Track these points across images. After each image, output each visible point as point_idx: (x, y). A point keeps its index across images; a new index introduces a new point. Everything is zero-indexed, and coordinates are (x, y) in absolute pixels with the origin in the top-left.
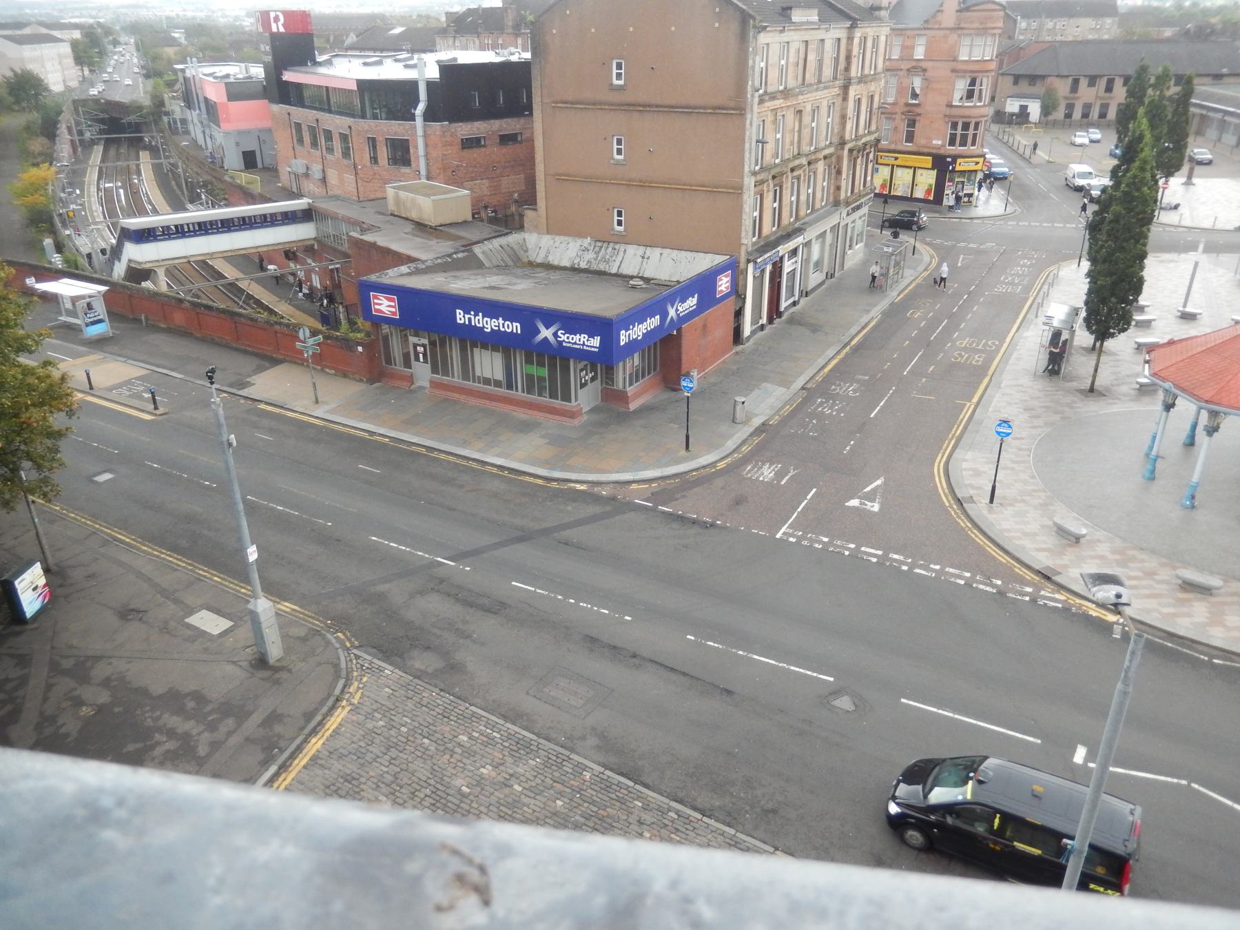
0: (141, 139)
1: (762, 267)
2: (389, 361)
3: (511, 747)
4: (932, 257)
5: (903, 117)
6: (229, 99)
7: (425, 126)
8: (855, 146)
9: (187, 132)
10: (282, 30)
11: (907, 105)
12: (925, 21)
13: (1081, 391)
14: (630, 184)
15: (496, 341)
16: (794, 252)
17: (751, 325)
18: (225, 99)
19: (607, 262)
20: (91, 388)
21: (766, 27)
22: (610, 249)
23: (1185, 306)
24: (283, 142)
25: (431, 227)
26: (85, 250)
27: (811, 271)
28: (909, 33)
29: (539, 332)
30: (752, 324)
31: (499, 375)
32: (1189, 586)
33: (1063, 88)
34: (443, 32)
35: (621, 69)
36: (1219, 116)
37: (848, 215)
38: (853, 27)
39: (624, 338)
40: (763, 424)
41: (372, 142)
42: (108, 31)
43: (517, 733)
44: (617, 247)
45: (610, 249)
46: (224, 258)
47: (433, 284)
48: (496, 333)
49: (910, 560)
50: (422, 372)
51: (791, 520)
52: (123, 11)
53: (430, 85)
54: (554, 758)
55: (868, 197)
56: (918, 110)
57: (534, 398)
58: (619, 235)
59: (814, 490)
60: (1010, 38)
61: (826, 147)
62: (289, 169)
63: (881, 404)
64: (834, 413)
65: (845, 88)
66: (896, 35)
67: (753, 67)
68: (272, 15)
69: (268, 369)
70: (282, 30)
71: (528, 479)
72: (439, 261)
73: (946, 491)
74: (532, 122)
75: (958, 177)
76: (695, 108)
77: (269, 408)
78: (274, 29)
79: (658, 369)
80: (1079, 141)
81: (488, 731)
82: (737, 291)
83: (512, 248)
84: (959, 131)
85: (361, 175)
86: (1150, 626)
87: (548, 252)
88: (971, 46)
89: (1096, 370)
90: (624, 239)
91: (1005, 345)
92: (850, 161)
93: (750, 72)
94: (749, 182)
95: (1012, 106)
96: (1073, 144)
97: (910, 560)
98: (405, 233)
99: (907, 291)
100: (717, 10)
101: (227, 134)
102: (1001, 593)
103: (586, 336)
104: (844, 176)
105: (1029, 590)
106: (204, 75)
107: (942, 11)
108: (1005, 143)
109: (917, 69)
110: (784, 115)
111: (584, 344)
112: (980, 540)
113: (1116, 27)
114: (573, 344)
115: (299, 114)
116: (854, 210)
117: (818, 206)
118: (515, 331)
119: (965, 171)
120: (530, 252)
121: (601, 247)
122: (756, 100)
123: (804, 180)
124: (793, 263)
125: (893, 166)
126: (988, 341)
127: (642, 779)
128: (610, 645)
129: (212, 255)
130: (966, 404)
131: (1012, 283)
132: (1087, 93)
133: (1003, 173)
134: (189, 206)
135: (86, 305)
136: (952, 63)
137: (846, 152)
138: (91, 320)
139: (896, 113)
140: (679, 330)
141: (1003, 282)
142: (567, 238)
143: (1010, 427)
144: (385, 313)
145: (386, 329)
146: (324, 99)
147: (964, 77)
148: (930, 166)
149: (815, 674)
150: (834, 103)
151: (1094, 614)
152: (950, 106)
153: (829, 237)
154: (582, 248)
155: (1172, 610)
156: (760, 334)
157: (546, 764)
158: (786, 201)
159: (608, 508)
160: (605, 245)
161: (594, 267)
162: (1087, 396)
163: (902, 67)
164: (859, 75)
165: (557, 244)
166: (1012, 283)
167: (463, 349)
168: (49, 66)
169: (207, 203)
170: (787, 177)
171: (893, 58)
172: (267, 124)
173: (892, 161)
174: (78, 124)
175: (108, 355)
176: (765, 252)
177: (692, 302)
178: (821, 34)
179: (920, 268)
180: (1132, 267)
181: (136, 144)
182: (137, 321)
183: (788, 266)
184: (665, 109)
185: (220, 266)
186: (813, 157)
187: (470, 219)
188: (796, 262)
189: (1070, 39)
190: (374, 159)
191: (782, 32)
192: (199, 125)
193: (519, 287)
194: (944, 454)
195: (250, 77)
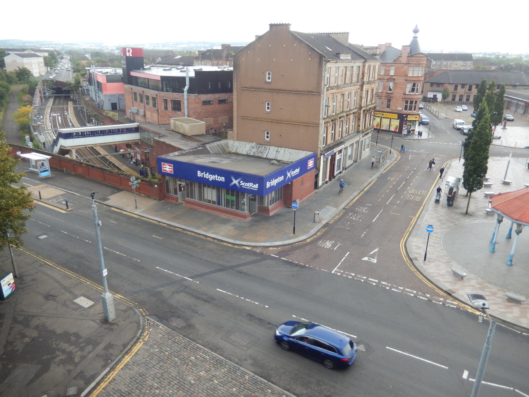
0: (69, 97)
2: (168, 192)
5: (386, 98)
6: (107, 82)
7: (188, 95)
9: (89, 95)
10: (131, 55)
11: (387, 93)
13: (462, 214)
14: (272, 121)
15: (214, 185)
16: (340, 151)
19: (262, 153)
20: (40, 199)
21: (330, 61)
22: (263, 148)
23: (505, 179)
24: (128, 100)
25: (188, 136)
26: (42, 141)
28: (387, 65)
29: (232, 181)
30: (323, 180)
31: (215, 199)
32: (511, 300)
33: (451, 88)
34: (197, 58)
36: (516, 101)
37: (363, 137)
39: (268, 185)
40: (327, 223)
41: (166, 101)
42: (59, 53)
44: (266, 147)
45: (263, 148)
47: (188, 160)
48: (214, 181)
49: (390, 285)
51: (338, 265)
52: (66, 45)
56: (391, 95)
57: (229, 209)
58: (267, 142)
61: (354, 109)
62: (130, 111)
63: (377, 216)
64: (357, 220)
65: (362, 86)
66: (382, 65)
67: (324, 76)
68: (127, 49)
69: (116, 193)
70: (131, 55)
71: (225, 244)
72: (191, 150)
73: (405, 255)
74: (233, 95)
75: (409, 123)
76: (300, 92)
77: (116, 210)
78: (128, 55)
80: (458, 110)
82: (316, 167)
83: (222, 146)
84: (409, 104)
85: (160, 114)
87: (237, 148)
88: (413, 71)
90: (269, 144)
91: (429, 193)
93: (323, 78)
94: (322, 122)
95: (430, 95)
98: (178, 139)
99: (388, 169)
100: (310, 53)
101: (106, 96)
102: (430, 300)
104: (361, 121)
105: (442, 299)
106: (98, 72)
107: (401, 57)
109: (391, 79)
111: (251, 187)
112: (420, 277)
113: (472, 65)
114: (247, 187)
115: (138, 89)
117: (350, 133)
118: (222, 181)
119: (411, 121)
120: (230, 148)
121: (260, 147)
124: (340, 156)
125: (381, 117)
127: (271, 379)
129: (96, 145)
132: (461, 91)
133: (427, 122)
134: (88, 124)
135: (41, 164)
136: (405, 77)
137: (362, 111)
138: (43, 170)
139: (382, 96)
140: (292, 182)
142: (245, 143)
143: (432, 228)
144: (167, 171)
145: (167, 178)
146: (147, 83)
151: (470, 311)
153: (355, 145)
155: (504, 310)
158: (337, 131)
160: (261, 146)
162: (464, 216)
163: (385, 78)
164: (368, 81)
165: (241, 145)
167: (200, 187)
168: (34, 66)
169: (95, 124)
170: (338, 121)
172: (122, 92)
173: (381, 116)
174: (44, 90)
175: (48, 185)
177: (297, 171)
178: (352, 64)
179: (393, 160)
180: (482, 162)
181: (67, 98)
182: (63, 171)
183: (338, 157)
184: (288, 92)
185: (98, 149)
186: (349, 113)
187: (205, 133)
188: (341, 155)
189: (453, 69)
190: (166, 108)
191: (336, 63)
192: (94, 92)
194: (404, 238)
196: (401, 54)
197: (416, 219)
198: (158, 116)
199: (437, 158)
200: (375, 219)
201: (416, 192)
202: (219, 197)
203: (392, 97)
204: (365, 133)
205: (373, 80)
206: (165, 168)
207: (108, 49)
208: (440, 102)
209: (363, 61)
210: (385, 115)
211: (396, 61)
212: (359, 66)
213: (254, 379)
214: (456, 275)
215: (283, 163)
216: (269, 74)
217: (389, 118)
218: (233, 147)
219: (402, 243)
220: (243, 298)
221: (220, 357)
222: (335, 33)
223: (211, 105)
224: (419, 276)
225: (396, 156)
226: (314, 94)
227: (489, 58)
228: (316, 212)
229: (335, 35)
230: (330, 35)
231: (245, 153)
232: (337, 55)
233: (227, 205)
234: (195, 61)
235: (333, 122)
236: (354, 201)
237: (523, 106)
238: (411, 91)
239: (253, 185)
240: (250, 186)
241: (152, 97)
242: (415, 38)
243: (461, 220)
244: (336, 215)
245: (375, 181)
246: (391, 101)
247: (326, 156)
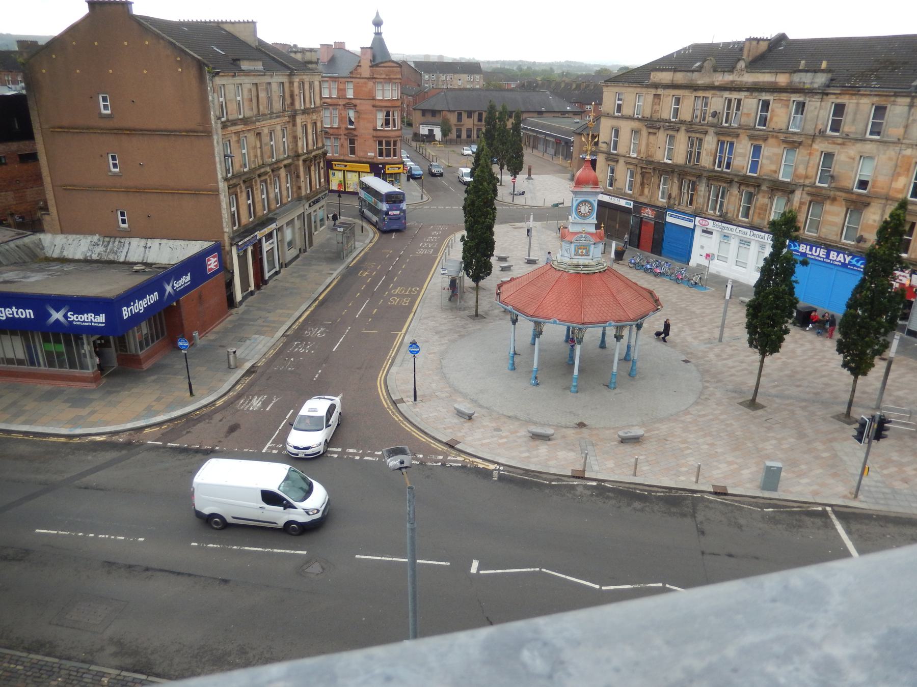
1: (244, 249)
3: (34, 674)
5: (346, 137)
8: (307, 158)
11: (347, 129)
13: (470, 317)
14: (127, 191)
16: (269, 236)
21: (218, 73)
22: (117, 243)
23: (529, 256)
29: (50, 315)
31: (21, 354)
32: (536, 437)
33: (453, 119)
35: (618, 104)
36: (543, 136)
38: (291, 75)
39: (126, 313)
40: (253, 366)
43: (40, 660)
44: (123, 240)
45: (117, 243)
49: (361, 452)
51: (274, 437)
54: (75, 674)
55: (324, 193)
56: (355, 133)
57: (56, 370)
58: (125, 230)
59: (292, 411)
60: (419, 85)
61: (285, 159)
63: (341, 341)
65: (293, 117)
66: (332, 81)
71: (52, 439)
73: (386, 397)
74: (35, 143)
76: (172, 132)
79: (166, 334)
80: (466, 152)
81: (12, 666)
82: (224, 267)
83: (28, 248)
84: (384, 147)
86: (515, 467)
87: (63, 248)
88: (383, 90)
89: (477, 302)
90: (129, 234)
91: (423, 290)
92: (305, 168)
95: (424, 130)
96: (463, 155)
97: (361, 452)
99: (358, 258)
100: (178, 59)
102: (422, 463)
103: (93, 315)
104: (302, 179)
105: (441, 457)
107: (360, 66)
109: (349, 105)
110: (246, 136)
111: (91, 322)
112: (408, 427)
114: (82, 322)
116: (315, 203)
117: (285, 201)
118: (28, 317)
119: (392, 174)
120: (45, 251)
121: (109, 242)
127: (153, 671)
128: (126, 565)
131: (427, 248)
132: (468, 123)
133: (419, 175)
136: (372, 101)
137: (301, 162)
139: (341, 135)
140: (178, 302)
141: (421, 247)
142: (78, 236)
143: (418, 347)
147: (381, 110)
149: (292, 552)
150: (286, 128)
151: (481, 466)
152: (375, 130)
154: (93, 243)
155: (526, 454)
156: (250, 299)
157: (68, 681)
158: (258, 198)
159: (124, 452)
160: (112, 240)
161: (105, 258)
163: (340, 103)
164: (303, 108)
165: (70, 242)
170: (256, 182)
173: (343, 168)
176: (245, 237)
177: (186, 279)
178: (267, 79)
179: (367, 241)
183: (266, 246)
184: (149, 133)
186: (275, 166)
188: (273, 243)
191: (234, 76)
194: (384, 371)
197: (403, 335)
202: (29, 349)
204: (313, 200)
205: (313, 106)
209: (288, 74)
210: (350, 166)
211: (353, 75)
213: (118, 680)
214: (460, 415)
216: (105, 99)
217: (356, 172)
218: (53, 247)
219: (381, 378)
220: (92, 535)
221: (47, 659)
222: (231, 23)
223: (4, 167)
224: (406, 428)
225: (371, 235)
226: (199, 134)
228: (229, 350)
229: (230, 25)
230: (222, 26)
231: (81, 258)
232: (235, 61)
233: (51, 364)
235: (247, 184)
236: (301, 320)
237: (553, 142)
239: (94, 318)
240: (90, 320)
242: (378, 34)
243: (470, 327)
244: (270, 349)
245: (337, 280)
246: (356, 142)
247: (242, 246)
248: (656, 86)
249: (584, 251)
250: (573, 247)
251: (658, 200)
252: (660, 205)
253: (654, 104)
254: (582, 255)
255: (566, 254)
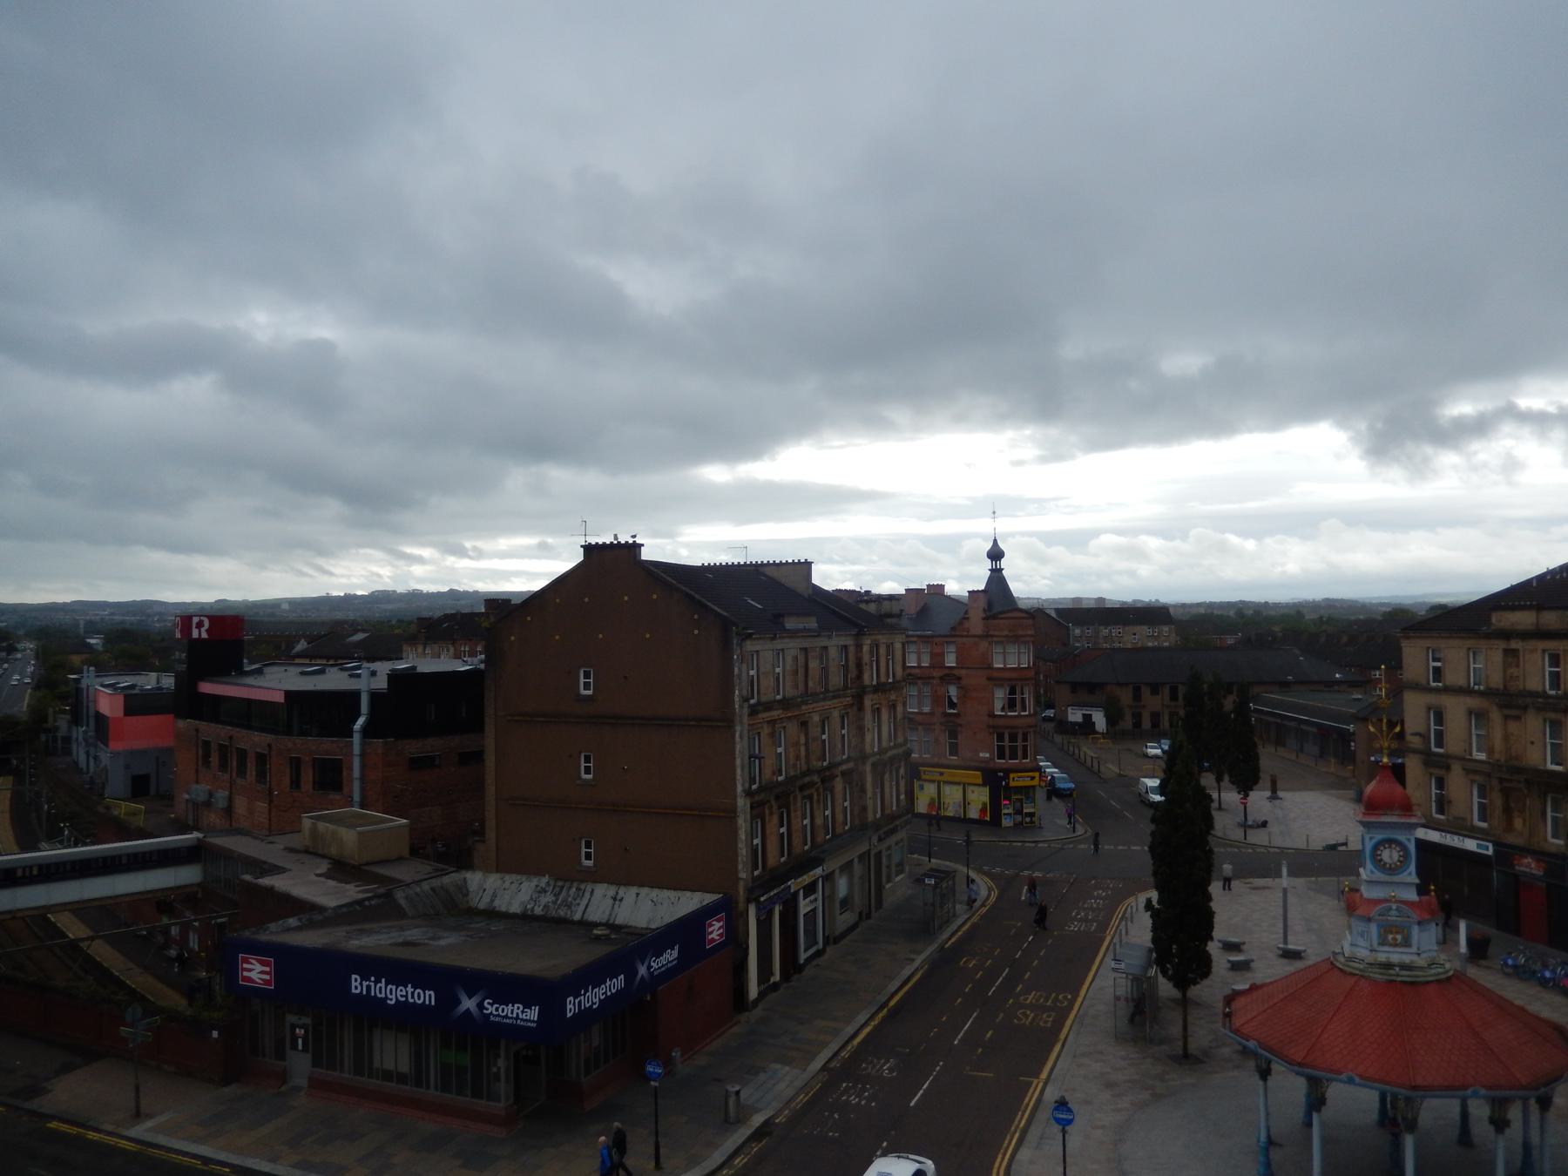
4: (990, 890)
6: (125, 715)
9: (68, 752)
10: (204, 635)
12: (952, 628)
16: (810, 889)
17: (758, 986)
18: (120, 713)
19: (569, 906)
21: (751, 635)
23: (1285, 942)
27: (838, 912)
28: (936, 640)
29: (459, 1002)
30: (760, 982)
31: (404, 1066)
33: (1126, 697)
34: (412, 640)
36: (1293, 724)
37: (880, 840)
39: (571, 1007)
40: (767, 1123)
41: (296, 764)
44: (583, 887)
46: (69, 910)
48: (402, 1006)
50: (300, 1065)
53: (375, 696)
60: (1065, 645)
62: (186, 796)
63: (925, 1087)
64: (863, 1103)
67: (740, 676)
68: (195, 620)
70: (204, 635)
75: (1015, 794)
77: (64, 1127)
78: (195, 634)
82: (735, 936)
84: (1007, 743)
87: (495, 895)
88: (1004, 654)
90: (594, 877)
91: (1080, 999)
93: (737, 681)
94: (742, 803)
95: (1075, 716)
96: (1146, 756)
98: (317, 875)
100: (696, 617)
104: (869, 794)
107: (968, 618)
108: (1077, 760)
109: (950, 677)
111: (517, 1018)
113: (1174, 635)
114: (504, 1017)
115: (214, 732)
118: (427, 1002)
121: (563, 887)
122: (746, 711)
123: (818, 801)
124: (811, 902)
125: (939, 782)
126: (1058, 995)
130: (1032, 1083)
131: (1085, 920)
132: (1152, 702)
137: (868, 768)
139: (934, 724)
142: (519, 877)
146: (250, 713)
148: (980, 781)
152: (992, 715)
153: (858, 869)
160: (568, 884)
163: (935, 674)
164: (875, 683)
165: (507, 884)
166: (1085, 920)
169: (69, 840)
170: (795, 798)
171: (923, 665)
177: (671, 956)
178: (823, 642)
183: (804, 906)
187: (406, 853)
188: (816, 900)
189: (1129, 646)
190: (296, 783)
191: (773, 639)
192: (84, 744)
193: (442, 943)
194: (1004, 1155)
195: (160, 688)
196: (966, 613)
198: (270, 811)
199: (1100, 892)
200: (919, 1095)
201: (1042, 1000)
203: (960, 725)
204: (885, 829)
206: (250, 970)
207: (165, 621)
208: (1103, 733)
212: (846, 647)
215: (631, 934)
216: (587, 675)
217: (958, 784)
226: (714, 724)
227: (1222, 615)
230: (761, 570)
232: (778, 618)
234: (406, 648)
238: (1006, 706)
241: (257, 753)
244: (798, 1094)
245: (922, 971)
248: (1506, 635)
249: (1399, 937)
250: (1374, 928)
251: (1546, 840)
252: (1553, 850)
253: (1506, 666)
254: (1396, 945)
255: (1361, 942)
